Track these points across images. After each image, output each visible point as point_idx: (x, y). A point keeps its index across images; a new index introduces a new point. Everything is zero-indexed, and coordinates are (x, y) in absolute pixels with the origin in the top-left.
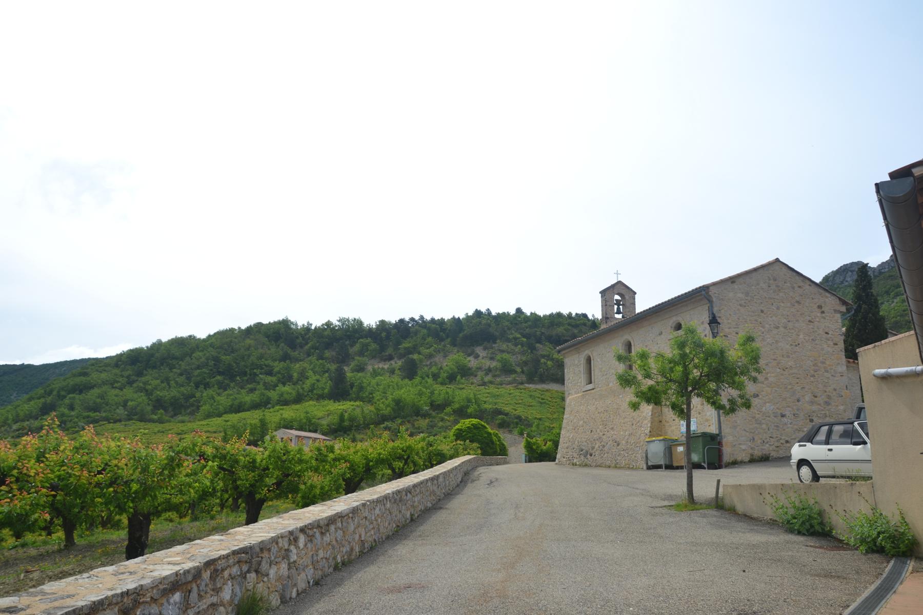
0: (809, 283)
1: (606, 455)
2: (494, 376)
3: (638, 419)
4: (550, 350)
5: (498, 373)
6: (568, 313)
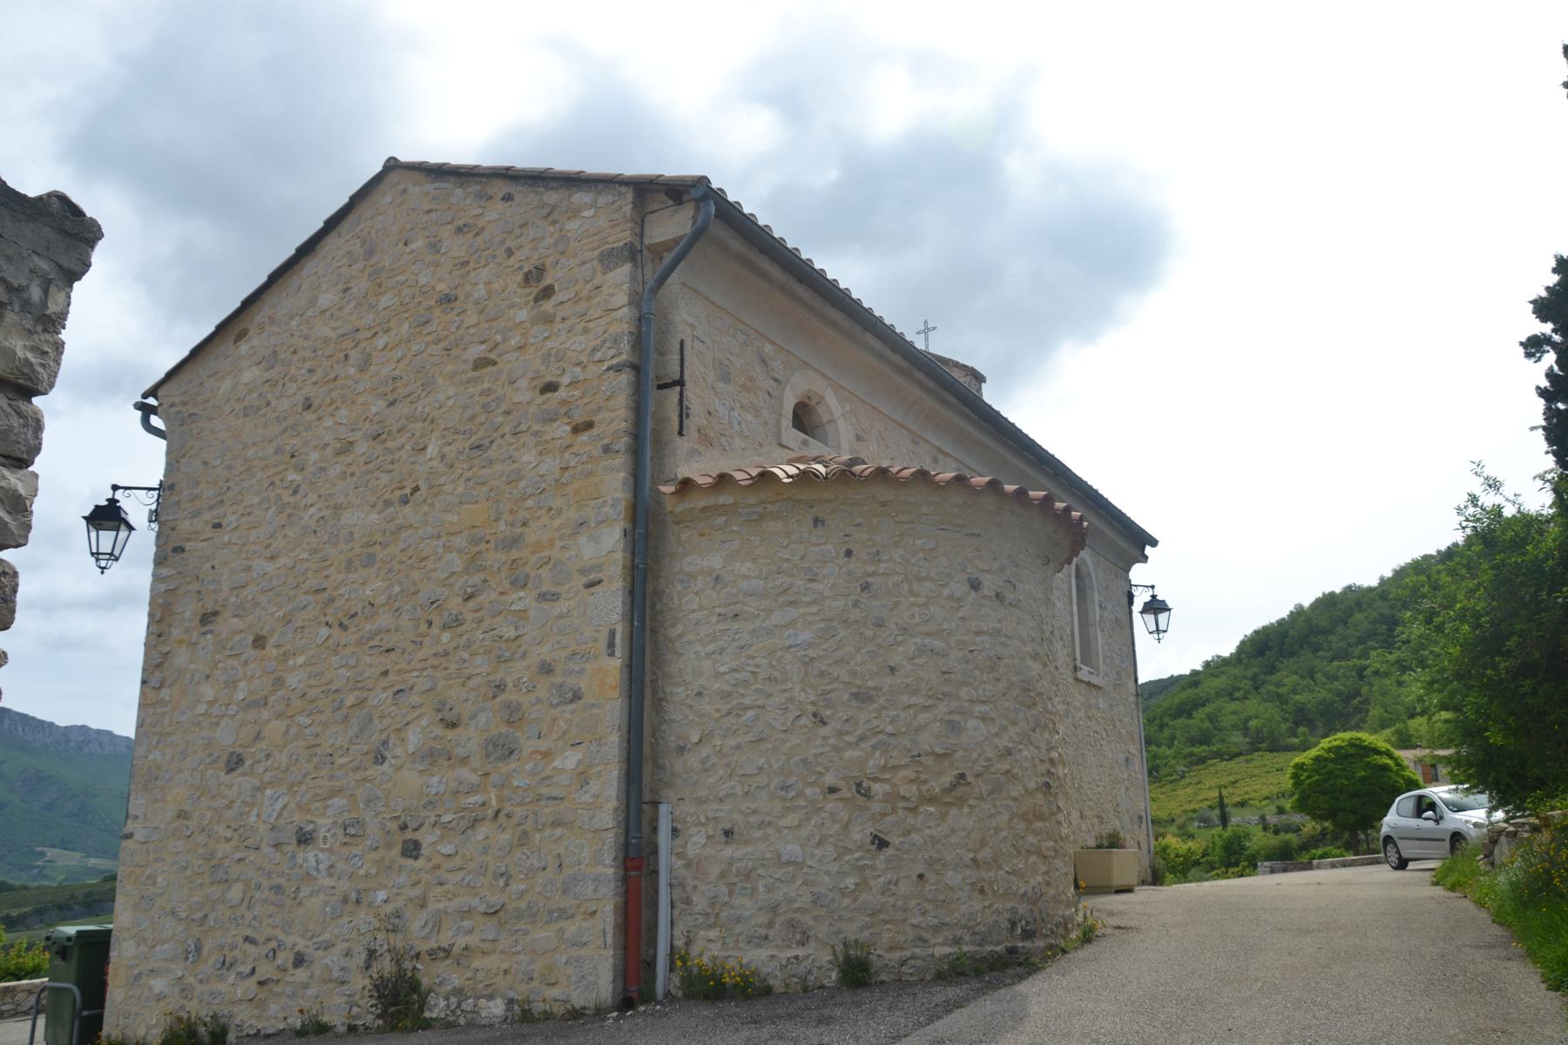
0: (501, 188)
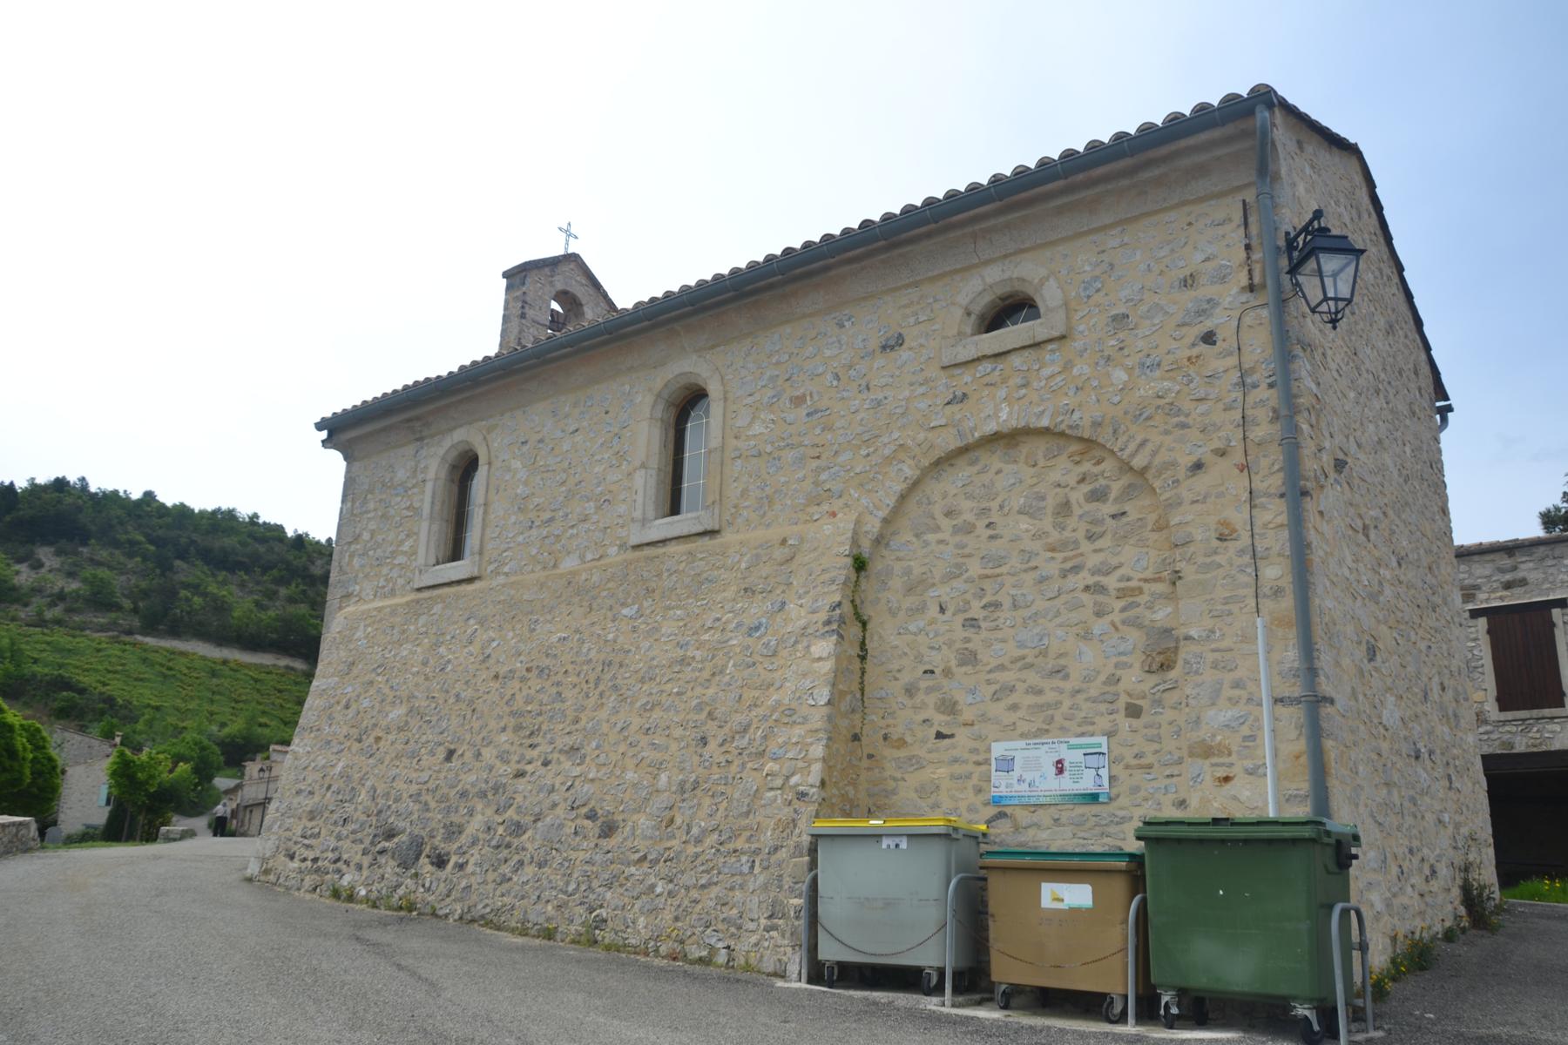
1: (530, 870)
2: (69, 610)
3: (739, 718)
4: (203, 576)
5: (78, 605)
6: (250, 513)
